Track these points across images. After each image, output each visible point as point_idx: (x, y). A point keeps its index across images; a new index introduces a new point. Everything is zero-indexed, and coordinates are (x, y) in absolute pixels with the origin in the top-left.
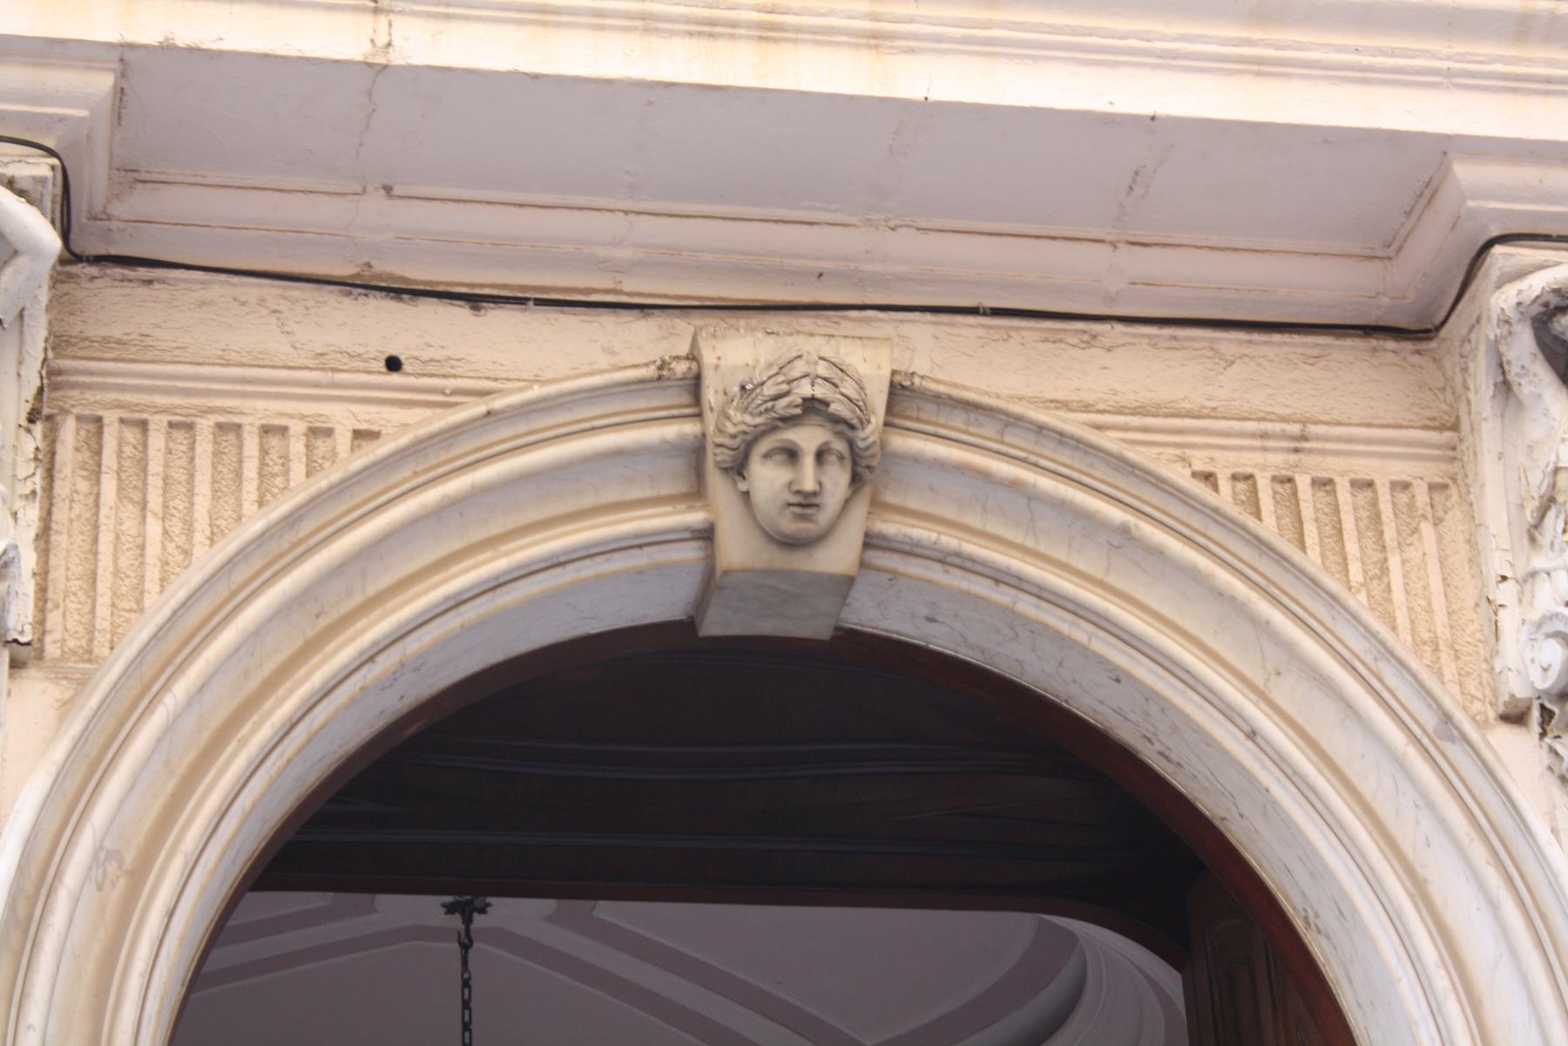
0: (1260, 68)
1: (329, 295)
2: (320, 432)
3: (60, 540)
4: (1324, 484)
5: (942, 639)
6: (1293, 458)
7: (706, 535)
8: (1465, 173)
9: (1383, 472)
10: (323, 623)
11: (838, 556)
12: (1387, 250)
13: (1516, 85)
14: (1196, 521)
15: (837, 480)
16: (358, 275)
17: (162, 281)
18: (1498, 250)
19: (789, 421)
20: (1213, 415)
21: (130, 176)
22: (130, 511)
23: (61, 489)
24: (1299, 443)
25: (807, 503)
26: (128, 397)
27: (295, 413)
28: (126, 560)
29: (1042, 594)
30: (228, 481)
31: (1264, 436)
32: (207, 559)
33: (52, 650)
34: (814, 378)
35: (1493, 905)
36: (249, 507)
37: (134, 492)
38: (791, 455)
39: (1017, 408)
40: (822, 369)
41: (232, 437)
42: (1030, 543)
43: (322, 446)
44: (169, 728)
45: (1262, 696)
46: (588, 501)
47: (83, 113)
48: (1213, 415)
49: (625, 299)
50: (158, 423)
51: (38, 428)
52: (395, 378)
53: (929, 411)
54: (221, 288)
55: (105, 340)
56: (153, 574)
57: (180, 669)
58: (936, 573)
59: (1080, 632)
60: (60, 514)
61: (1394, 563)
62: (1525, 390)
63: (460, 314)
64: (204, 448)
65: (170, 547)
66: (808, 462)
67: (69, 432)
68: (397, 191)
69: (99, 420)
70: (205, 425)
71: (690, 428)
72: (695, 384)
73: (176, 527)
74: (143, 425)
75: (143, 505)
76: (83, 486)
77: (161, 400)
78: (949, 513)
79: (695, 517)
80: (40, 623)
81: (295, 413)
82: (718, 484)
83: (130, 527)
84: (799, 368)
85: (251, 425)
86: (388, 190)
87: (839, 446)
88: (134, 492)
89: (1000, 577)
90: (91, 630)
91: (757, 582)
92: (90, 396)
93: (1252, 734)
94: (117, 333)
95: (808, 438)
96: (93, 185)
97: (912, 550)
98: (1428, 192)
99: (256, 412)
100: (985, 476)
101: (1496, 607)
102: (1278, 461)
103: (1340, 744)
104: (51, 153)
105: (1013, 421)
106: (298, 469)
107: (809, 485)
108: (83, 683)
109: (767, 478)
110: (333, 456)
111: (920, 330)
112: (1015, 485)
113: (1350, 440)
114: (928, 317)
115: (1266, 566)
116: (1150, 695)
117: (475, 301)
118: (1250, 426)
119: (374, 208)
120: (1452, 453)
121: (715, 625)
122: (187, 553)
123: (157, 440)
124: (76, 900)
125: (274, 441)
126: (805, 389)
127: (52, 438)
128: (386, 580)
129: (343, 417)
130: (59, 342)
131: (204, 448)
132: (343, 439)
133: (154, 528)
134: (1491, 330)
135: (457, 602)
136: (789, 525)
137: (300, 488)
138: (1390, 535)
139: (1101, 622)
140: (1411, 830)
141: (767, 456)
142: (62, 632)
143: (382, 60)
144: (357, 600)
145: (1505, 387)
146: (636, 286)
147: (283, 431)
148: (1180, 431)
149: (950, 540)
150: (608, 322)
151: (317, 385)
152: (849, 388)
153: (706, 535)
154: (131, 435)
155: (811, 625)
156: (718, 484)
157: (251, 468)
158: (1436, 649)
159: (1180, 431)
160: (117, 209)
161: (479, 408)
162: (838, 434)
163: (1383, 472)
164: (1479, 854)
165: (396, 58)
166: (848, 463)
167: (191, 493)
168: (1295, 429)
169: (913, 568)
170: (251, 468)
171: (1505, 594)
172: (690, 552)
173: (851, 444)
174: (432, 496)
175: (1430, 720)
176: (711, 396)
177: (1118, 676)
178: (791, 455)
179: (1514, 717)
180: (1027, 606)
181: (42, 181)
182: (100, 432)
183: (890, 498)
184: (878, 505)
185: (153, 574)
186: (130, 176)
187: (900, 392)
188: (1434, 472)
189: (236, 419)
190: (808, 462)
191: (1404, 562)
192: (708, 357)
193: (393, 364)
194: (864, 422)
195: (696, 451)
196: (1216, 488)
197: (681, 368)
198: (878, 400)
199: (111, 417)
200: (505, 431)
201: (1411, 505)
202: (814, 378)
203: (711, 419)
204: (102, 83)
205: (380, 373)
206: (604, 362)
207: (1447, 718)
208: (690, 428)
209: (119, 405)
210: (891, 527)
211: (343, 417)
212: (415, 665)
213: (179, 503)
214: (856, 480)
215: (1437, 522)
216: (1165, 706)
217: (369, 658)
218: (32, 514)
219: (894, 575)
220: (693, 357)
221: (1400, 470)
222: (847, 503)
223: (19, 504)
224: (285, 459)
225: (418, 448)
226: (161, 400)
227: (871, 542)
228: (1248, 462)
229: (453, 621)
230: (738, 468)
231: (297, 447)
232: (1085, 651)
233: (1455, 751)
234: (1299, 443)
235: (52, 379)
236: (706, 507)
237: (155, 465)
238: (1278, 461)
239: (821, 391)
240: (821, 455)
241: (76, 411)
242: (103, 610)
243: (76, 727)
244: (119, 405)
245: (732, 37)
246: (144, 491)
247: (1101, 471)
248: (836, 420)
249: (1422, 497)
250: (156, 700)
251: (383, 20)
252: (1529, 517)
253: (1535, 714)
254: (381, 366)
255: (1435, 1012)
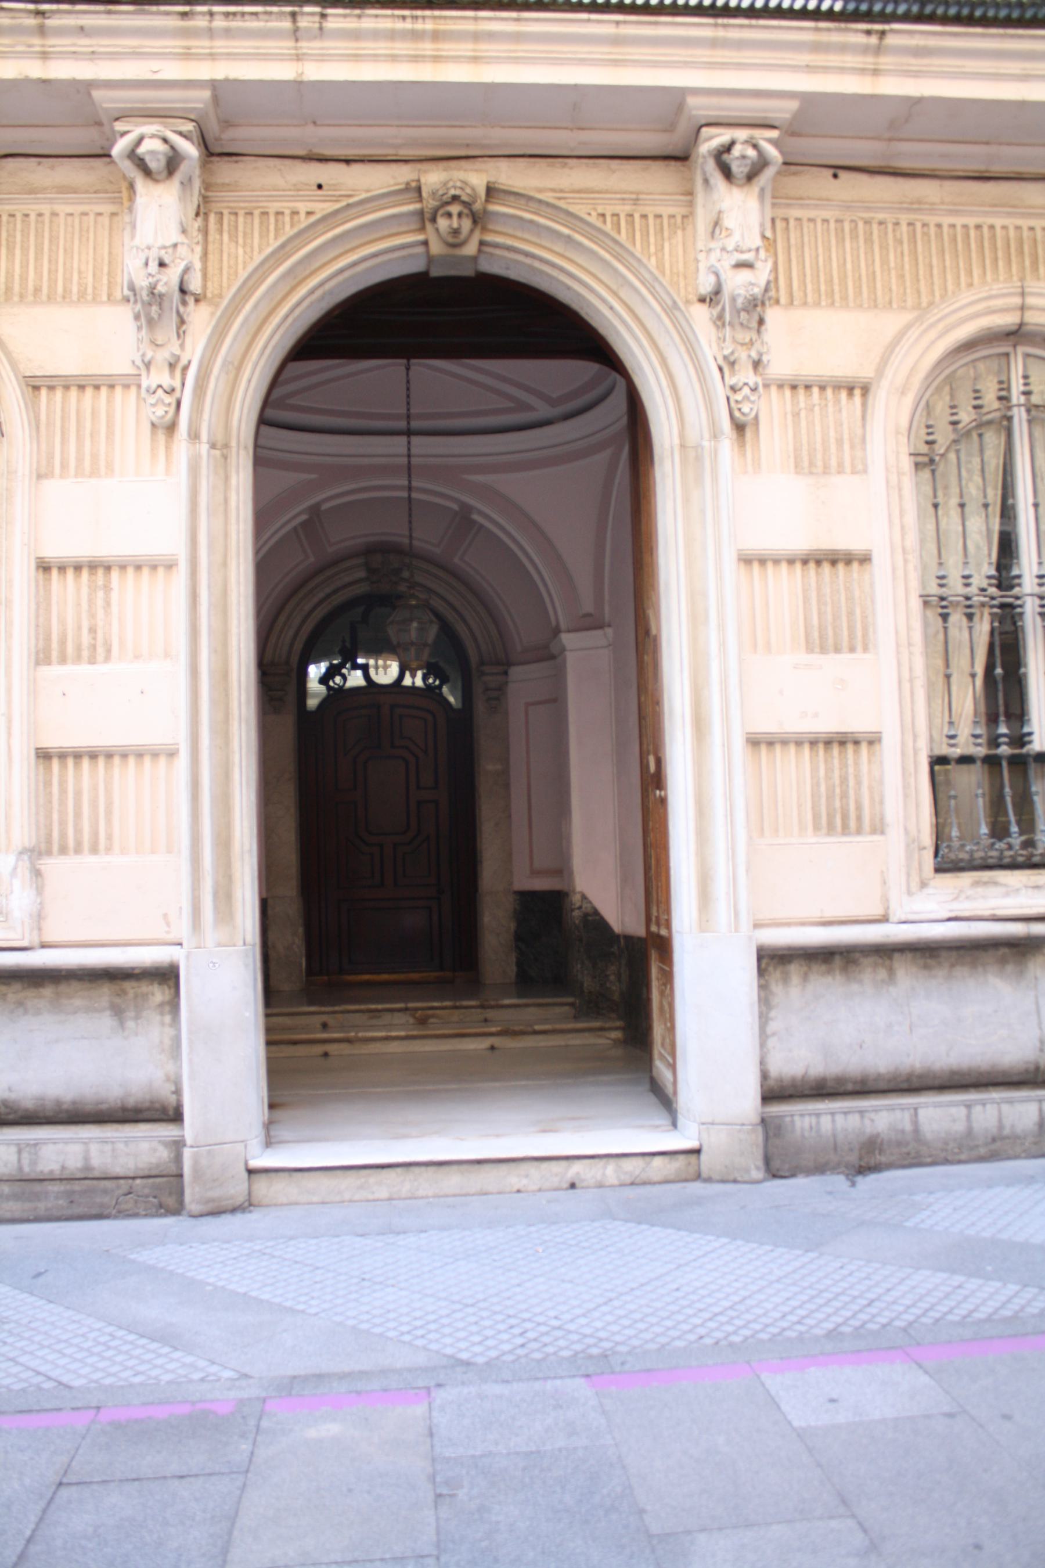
0: (616, 63)
1: (298, 163)
2: (294, 213)
3: (210, 257)
4: (644, 216)
5: (513, 274)
6: (634, 207)
7: (425, 243)
8: (691, 101)
9: (672, 210)
10: (298, 280)
11: (470, 249)
12: (671, 128)
13: (711, 66)
14: (594, 233)
15: (467, 224)
16: (307, 155)
17: (242, 161)
18: (704, 130)
19: (447, 203)
20: (607, 192)
21: (227, 124)
22: (233, 245)
23: (211, 238)
24: (636, 201)
25: (456, 232)
26: (232, 205)
27: (286, 206)
28: (232, 262)
29: (541, 260)
30: (264, 234)
31: (623, 199)
32: (258, 259)
33: (209, 295)
34: (455, 187)
35: (686, 366)
36: (271, 241)
37: (233, 237)
38: (449, 215)
39: (532, 194)
40: (459, 184)
41: (266, 216)
42: (538, 241)
43: (296, 217)
44: (246, 320)
45: (615, 294)
46: (386, 233)
47: (201, 106)
48: (607, 192)
49: (398, 158)
50: (241, 213)
51: (200, 219)
52: (320, 192)
53: (502, 195)
54: (261, 163)
55: (223, 185)
56: (240, 267)
57: (247, 300)
58: (506, 254)
59: (555, 273)
60: (210, 247)
61: (667, 245)
62: (712, 181)
63: (342, 167)
64: (257, 221)
65: (247, 257)
66: (455, 218)
67: (212, 218)
68: (318, 122)
69: (221, 214)
70: (257, 213)
71: (418, 206)
72: (419, 189)
73: (248, 250)
74: (236, 214)
75: (237, 242)
76: (218, 237)
77: (242, 205)
78: (510, 231)
79: (421, 237)
80: (205, 287)
81: (286, 206)
82: (429, 226)
83: (233, 250)
84: (451, 184)
85: (272, 211)
86: (314, 123)
87: (466, 211)
88: (233, 237)
89: (527, 254)
90: (221, 286)
91: (443, 259)
92: (219, 205)
93: (611, 308)
94: (227, 181)
95: (455, 209)
96: (213, 128)
97: (496, 246)
98: (681, 106)
99: (274, 207)
100: (521, 219)
101: (697, 261)
102: (628, 208)
103: (641, 311)
104: (192, 120)
105: (530, 198)
106: (288, 227)
107: (455, 225)
108: (217, 305)
109: (443, 223)
110: (299, 221)
111: (503, 164)
112: (531, 222)
113: (654, 200)
114: (506, 159)
115: (617, 248)
116: (579, 295)
117: (348, 161)
118: (618, 196)
119: (310, 130)
120: (691, 204)
121: (435, 273)
122: (251, 258)
123: (241, 219)
124: (217, 379)
125: (280, 217)
126: (453, 192)
127: (206, 219)
128: (317, 265)
129: (302, 207)
130: (207, 186)
131: (257, 221)
132: (303, 215)
133: (241, 251)
134: (700, 160)
135: (341, 271)
136: (451, 240)
137: (289, 231)
138: (666, 234)
139: (562, 270)
140: (662, 341)
141: (442, 215)
142: (212, 289)
143: (299, 79)
144: (308, 272)
145: (706, 181)
146: (404, 153)
147: (282, 213)
148: (593, 199)
149: (509, 242)
150: (394, 167)
151: (293, 196)
152: (468, 191)
153: (425, 243)
154: (233, 218)
155: (468, 272)
156: (429, 226)
157: (272, 227)
158: (678, 276)
159: (593, 199)
160: (224, 136)
161: (343, 204)
162: (465, 207)
163: (665, 211)
164: (682, 349)
165: (305, 78)
166: (470, 217)
167: (252, 238)
168: (634, 196)
169: (498, 252)
170: (272, 227)
171: (701, 257)
172: (421, 249)
173: (471, 211)
174: (330, 235)
175: (670, 303)
176: (424, 194)
177: (569, 288)
178: (449, 215)
179: (702, 300)
180: (537, 264)
181: (190, 132)
182: (221, 219)
183: (490, 227)
184: (484, 229)
185: (240, 267)
186: (227, 124)
187: (491, 191)
188: (684, 211)
189: (267, 210)
190: (455, 218)
191: (670, 244)
192: (423, 180)
193: (320, 187)
194: (474, 202)
195: (421, 213)
196: (605, 222)
197: (414, 184)
198: (482, 192)
199: (226, 212)
200: (354, 211)
201: (675, 224)
202: (455, 187)
203: (424, 202)
204: (206, 94)
205: (313, 190)
206: (392, 182)
207: (675, 302)
208: (418, 206)
209: (228, 207)
210: (489, 238)
211: (302, 207)
212: (331, 292)
213: (249, 241)
214: (475, 222)
215: (684, 229)
216: (584, 298)
217: (312, 292)
218: (198, 249)
219: (492, 255)
220: (419, 181)
221: (672, 210)
222: (472, 231)
223: (194, 246)
224: (284, 223)
225: (324, 219)
226: (242, 205)
227: (482, 243)
228: (617, 209)
229: (341, 278)
230: (434, 220)
231: (287, 219)
232: (558, 280)
233: (677, 313)
234: (636, 201)
235: (205, 199)
236: (425, 233)
237: (241, 228)
238: (628, 208)
239: (458, 192)
240: (460, 215)
241: (215, 210)
242: (225, 280)
243: (213, 323)
244: (228, 207)
245: (424, 61)
246: (237, 237)
247: (562, 216)
248: (464, 203)
249: (679, 219)
250: (240, 311)
251: (300, 63)
252: (710, 229)
253: (708, 300)
254: (315, 187)
255: (665, 403)
